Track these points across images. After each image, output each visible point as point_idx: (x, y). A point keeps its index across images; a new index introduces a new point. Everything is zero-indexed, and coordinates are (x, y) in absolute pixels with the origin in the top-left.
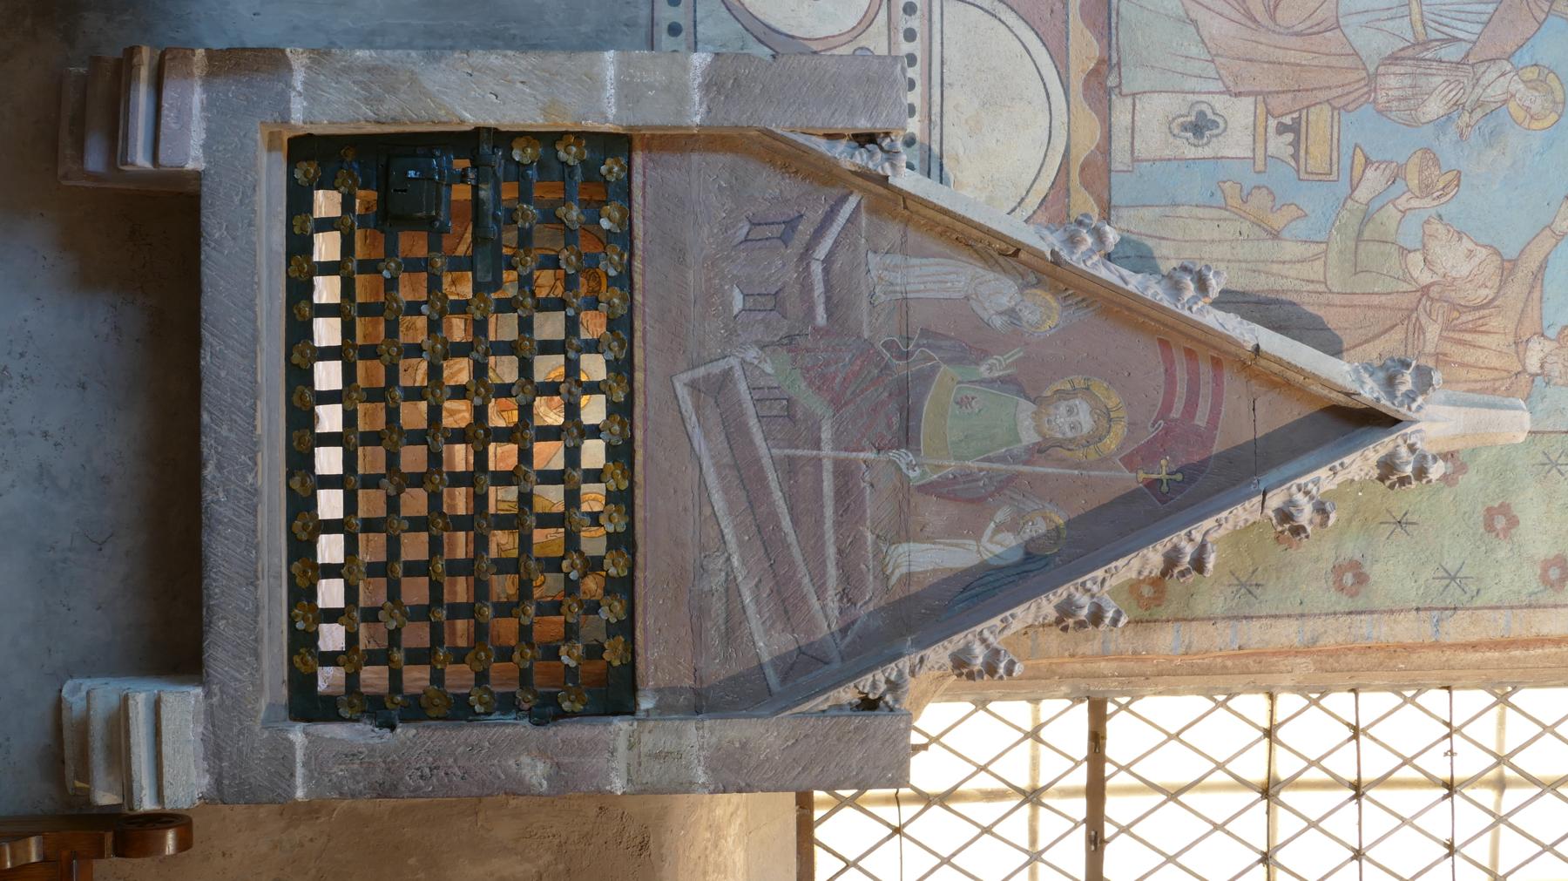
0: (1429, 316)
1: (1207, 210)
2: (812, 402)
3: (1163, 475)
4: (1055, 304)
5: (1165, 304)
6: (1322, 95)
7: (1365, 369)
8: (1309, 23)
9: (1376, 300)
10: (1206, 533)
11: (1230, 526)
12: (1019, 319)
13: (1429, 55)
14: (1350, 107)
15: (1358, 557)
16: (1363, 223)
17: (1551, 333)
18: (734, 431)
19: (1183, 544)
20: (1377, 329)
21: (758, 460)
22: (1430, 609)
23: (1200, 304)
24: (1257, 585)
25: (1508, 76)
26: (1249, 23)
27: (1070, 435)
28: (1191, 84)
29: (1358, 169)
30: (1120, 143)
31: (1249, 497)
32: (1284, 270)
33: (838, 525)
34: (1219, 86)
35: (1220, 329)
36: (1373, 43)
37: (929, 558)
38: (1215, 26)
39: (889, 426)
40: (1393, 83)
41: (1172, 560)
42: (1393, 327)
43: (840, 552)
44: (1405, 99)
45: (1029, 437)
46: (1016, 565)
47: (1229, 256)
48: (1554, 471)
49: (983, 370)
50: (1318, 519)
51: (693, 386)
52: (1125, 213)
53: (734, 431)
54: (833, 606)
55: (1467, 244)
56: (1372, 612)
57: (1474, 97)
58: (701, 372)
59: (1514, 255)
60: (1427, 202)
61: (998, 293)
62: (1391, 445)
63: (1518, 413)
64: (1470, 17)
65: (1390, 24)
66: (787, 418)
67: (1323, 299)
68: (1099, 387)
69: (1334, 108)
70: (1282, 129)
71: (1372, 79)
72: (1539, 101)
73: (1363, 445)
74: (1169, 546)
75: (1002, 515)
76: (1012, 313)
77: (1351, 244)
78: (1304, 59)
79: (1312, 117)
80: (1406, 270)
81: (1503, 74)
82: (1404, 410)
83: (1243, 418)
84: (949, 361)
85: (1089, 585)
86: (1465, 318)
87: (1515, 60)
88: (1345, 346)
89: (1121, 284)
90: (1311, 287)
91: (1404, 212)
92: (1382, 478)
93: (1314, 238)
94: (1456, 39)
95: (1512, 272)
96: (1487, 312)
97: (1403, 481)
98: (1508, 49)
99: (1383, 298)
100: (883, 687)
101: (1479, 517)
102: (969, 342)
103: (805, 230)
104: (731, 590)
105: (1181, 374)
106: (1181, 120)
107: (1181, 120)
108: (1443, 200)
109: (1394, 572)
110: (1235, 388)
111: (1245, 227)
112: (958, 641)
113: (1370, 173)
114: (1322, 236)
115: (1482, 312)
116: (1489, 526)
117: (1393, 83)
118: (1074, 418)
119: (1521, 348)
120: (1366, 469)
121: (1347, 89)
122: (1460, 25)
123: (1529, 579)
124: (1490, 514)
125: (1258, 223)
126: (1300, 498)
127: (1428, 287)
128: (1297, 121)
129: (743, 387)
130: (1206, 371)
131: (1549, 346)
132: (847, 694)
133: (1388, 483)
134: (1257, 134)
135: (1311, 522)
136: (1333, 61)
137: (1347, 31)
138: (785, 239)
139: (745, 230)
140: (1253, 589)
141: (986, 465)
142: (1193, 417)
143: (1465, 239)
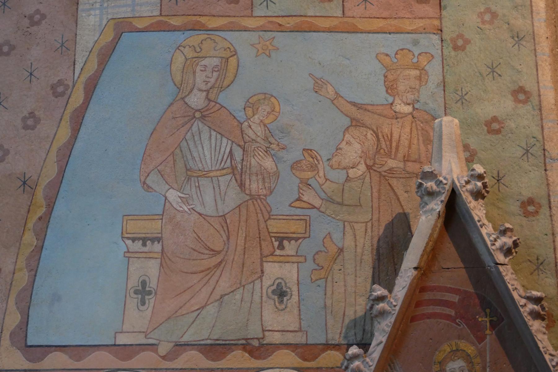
0: (383, 165)
1: (328, 289)
3: (487, 319)
5: (393, 320)
6: (262, 225)
7: (423, 207)
8: (222, 232)
9: (375, 194)
10: (520, 296)
11: (515, 283)
13: (239, 166)
14: (269, 209)
15: (518, 203)
16: (332, 201)
17: (390, 99)
19: (527, 310)
20: (392, 194)
22: (545, 164)
23: (392, 300)
24: (538, 259)
25: (251, 124)
26: (222, 265)
28: (257, 298)
29: (305, 205)
30: (291, 338)
31: (500, 273)
32: (360, 245)
34: (258, 282)
35: (406, 289)
36: (233, 197)
38: (224, 285)
40: (255, 186)
41: (536, 315)
42: (390, 185)
44: (264, 179)
47: (353, 276)
48: (466, 97)
50: (509, 234)
52: (330, 336)
55: (343, 145)
56: (549, 196)
57: (262, 142)
59: (348, 119)
60: (320, 167)
62: (467, 194)
63: (443, 123)
64: (218, 144)
65: (222, 188)
67: (376, 224)
69: (269, 218)
70: (281, 247)
71: (252, 197)
72: (264, 107)
73: (468, 211)
74: (529, 317)
77: (345, 208)
78: (242, 235)
79: (275, 231)
80: (358, 178)
81: (250, 127)
82: (447, 187)
83: (453, 274)
85: (554, 364)
86: (384, 146)
87: (242, 121)
88: (401, 211)
89: (382, 346)
90: (369, 230)
91: (327, 180)
92: (483, 197)
93: (342, 229)
94: (231, 152)
95: (357, 121)
96: (380, 135)
98: (236, 124)
99: (374, 190)
101: (493, 137)
105: (430, 309)
106: (277, 303)
107: (277, 303)
108: (319, 158)
109: (526, 183)
110: (438, 279)
111: (336, 267)
113: (305, 198)
114: (341, 224)
115: (380, 137)
116: (498, 132)
117: (255, 186)
119: (399, 116)
120: (480, 207)
121: (259, 211)
122: (223, 150)
123: (523, 109)
124: (491, 131)
126: (498, 244)
127: (367, 166)
128: (277, 238)
130: (427, 296)
131: (397, 101)
133: (486, 194)
134: (285, 261)
135: (510, 237)
136: (243, 218)
137: (226, 211)
140: (540, 262)
142: (454, 303)
143: (341, 146)
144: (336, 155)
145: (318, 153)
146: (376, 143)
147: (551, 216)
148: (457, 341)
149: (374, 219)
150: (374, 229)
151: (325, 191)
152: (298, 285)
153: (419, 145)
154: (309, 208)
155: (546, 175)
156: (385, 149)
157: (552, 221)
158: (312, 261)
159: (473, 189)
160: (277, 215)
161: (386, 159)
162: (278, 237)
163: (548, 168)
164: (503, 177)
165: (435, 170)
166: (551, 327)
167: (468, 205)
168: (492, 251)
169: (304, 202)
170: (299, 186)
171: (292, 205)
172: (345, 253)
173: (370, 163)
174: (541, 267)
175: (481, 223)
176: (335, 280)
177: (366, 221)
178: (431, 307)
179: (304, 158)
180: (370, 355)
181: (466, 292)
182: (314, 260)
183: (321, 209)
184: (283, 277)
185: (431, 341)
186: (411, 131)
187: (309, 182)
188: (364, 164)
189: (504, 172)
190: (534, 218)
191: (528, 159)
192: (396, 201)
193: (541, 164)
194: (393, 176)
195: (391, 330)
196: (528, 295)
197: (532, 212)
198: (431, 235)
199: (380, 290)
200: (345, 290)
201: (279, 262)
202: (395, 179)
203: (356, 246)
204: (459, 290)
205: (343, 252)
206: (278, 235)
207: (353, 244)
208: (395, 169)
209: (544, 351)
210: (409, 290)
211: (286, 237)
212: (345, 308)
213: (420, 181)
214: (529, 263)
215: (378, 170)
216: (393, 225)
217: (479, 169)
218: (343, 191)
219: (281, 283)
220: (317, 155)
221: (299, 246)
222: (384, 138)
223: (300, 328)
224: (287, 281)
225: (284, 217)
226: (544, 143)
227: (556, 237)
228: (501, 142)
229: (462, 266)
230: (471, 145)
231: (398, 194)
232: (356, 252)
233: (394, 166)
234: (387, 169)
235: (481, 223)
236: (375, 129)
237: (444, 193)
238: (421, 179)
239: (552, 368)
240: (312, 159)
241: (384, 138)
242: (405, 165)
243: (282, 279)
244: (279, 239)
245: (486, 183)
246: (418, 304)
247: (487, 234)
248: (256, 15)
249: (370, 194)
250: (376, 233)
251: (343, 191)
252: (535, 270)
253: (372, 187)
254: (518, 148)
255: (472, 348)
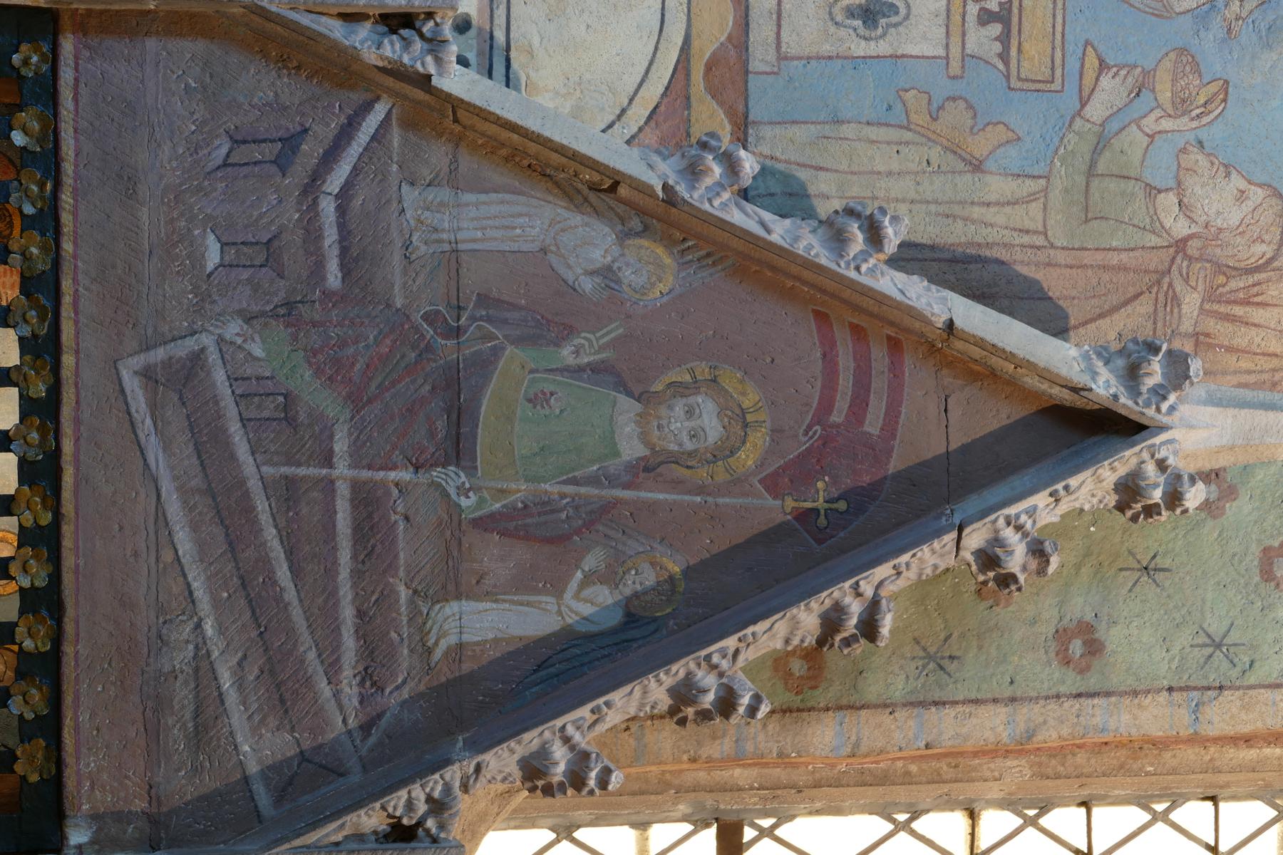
0: (1187, 280)
1: (883, 130)
2: (321, 399)
3: (820, 504)
4: (668, 261)
5: (823, 261)
7: (1099, 355)
9: (1114, 259)
10: (880, 585)
11: (911, 575)
12: (619, 282)
15: (1089, 617)
16: (1097, 151)
18: (208, 443)
19: (848, 600)
20: (1115, 299)
21: (242, 483)
23: (872, 261)
27: (689, 446)
30: (761, 33)
31: (939, 533)
33: (357, 575)
35: (899, 297)
37: (486, 623)
39: (432, 434)
41: (832, 621)
43: (360, 614)
45: (631, 449)
46: (613, 631)
47: (912, 195)
49: (566, 354)
50: (1033, 564)
51: (147, 374)
52: (767, 132)
53: (208, 443)
54: (351, 692)
55: (1237, 182)
56: (1108, 694)
58: (160, 354)
61: (588, 244)
62: (1134, 461)
66: (283, 420)
67: (1042, 256)
68: (730, 380)
70: (986, 17)
73: (1093, 461)
74: (828, 603)
75: (592, 561)
76: (607, 273)
77: (1081, 180)
82: (1151, 412)
83: (932, 422)
84: (518, 341)
88: (1072, 322)
89: (761, 232)
90: (1026, 239)
91: (1151, 137)
92: (1121, 507)
93: (1029, 171)
97: (1150, 511)
99: (1124, 256)
100: (422, 808)
101: (1253, 560)
102: (549, 320)
103: (311, 150)
104: (202, 669)
108: (1205, 120)
109: (1140, 638)
110: (920, 385)
111: (935, 153)
112: (530, 740)
113: (1106, 81)
114: (1040, 169)
115: (1257, 277)
118: (696, 422)
120: (1100, 494)
125: (953, 149)
126: (1009, 534)
127: (1185, 240)
129: (220, 376)
130: (879, 356)
132: (371, 819)
133: (1129, 513)
135: (1024, 568)
138: (282, 163)
139: (224, 150)
140: (946, 663)
141: (570, 489)
142: (861, 422)
143: (1234, 175)
144: (1212, 164)
145: (1216, 117)
146: (1242, 265)
147: (1058, 696)
148: (768, 424)
149: (1052, 252)
150: (1029, 251)
151: (1124, 133)
152: (891, 56)
153: (1235, 372)
154: (1080, 91)
155: (1159, 691)
156: (1227, 288)
157: (1047, 698)
158: (951, 94)
159: (1145, 479)
160: (1064, 9)
161: (1199, 289)
162: (1010, 10)
163: (1176, 696)
164: (1154, 581)
165: (1192, 384)
166: (786, 684)
167: (1106, 463)
168: (993, 517)
169: (1097, 79)
170: (1136, 67)
171: (1089, 49)
172: (969, 176)
173: (1193, 247)
174: (932, 666)
175: (1062, 493)
176: (903, 149)
177: (1050, 233)
178: (852, 365)
179: (1205, 81)
180: (737, 204)
181: (889, 452)
182: (954, 99)
183: (1078, 119)
184: (912, 20)
185: (768, 360)
186: (1269, 355)
187: (1145, 93)
188: (1190, 232)
189: (1167, 584)
190: (1053, 655)
191: (1198, 646)
192: (1098, 311)
193: (1185, 677)
194: (1161, 309)
195: (799, 255)
196: (884, 602)
197: (1067, 649)
198: (1031, 366)
199: (896, 234)
200: (879, 173)
201: (948, 11)
202: (1151, 310)
203: (988, 205)
204: (893, 436)
205: (973, 172)
206: (1015, 11)
207: (993, 197)
208: (1176, 310)
209: (745, 636)
210: (899, 306)
211: (1009, 31)
212: (836, 171)
213: (1164, 347)
214: (942, 636)
215: (1174, 268)
216: (1039, 299)
217: (1195, 497)
218: (1124, 177)
219: (897, 13)
220: (1212, 116)
221: (987, 62)
222: (1254, 285)
223: (786, 58)
224: (901, 29)
225: (1059, 28)
226: (1238, 688)
227: (1006, 705)
228: (1242, 581)
229: (953, 446)
230: (1234, 504)
231: (1116, 316)
232: (972, 203)
233: (1185, 308)
234: (1178, 289)
235: (1062, 493)
236: (1276, 264)
237: (1137, 404)
238: (1170, 352)
239: (703, 653)
240: (1202, 102)
241: (1254, 285)
242: (1186, 335)
243: (907, 17)
244: (1005, 12)
245: (1160, 514)
246: (858, 332)
247: (1035, 508)
248: (920, 831)
249: (1114, 244)
250: (1019, 255)
251: (1124, 177)
252: (925, 650)
253: (1132, 250)
254: (1226, 623)
255: (750, 463)
